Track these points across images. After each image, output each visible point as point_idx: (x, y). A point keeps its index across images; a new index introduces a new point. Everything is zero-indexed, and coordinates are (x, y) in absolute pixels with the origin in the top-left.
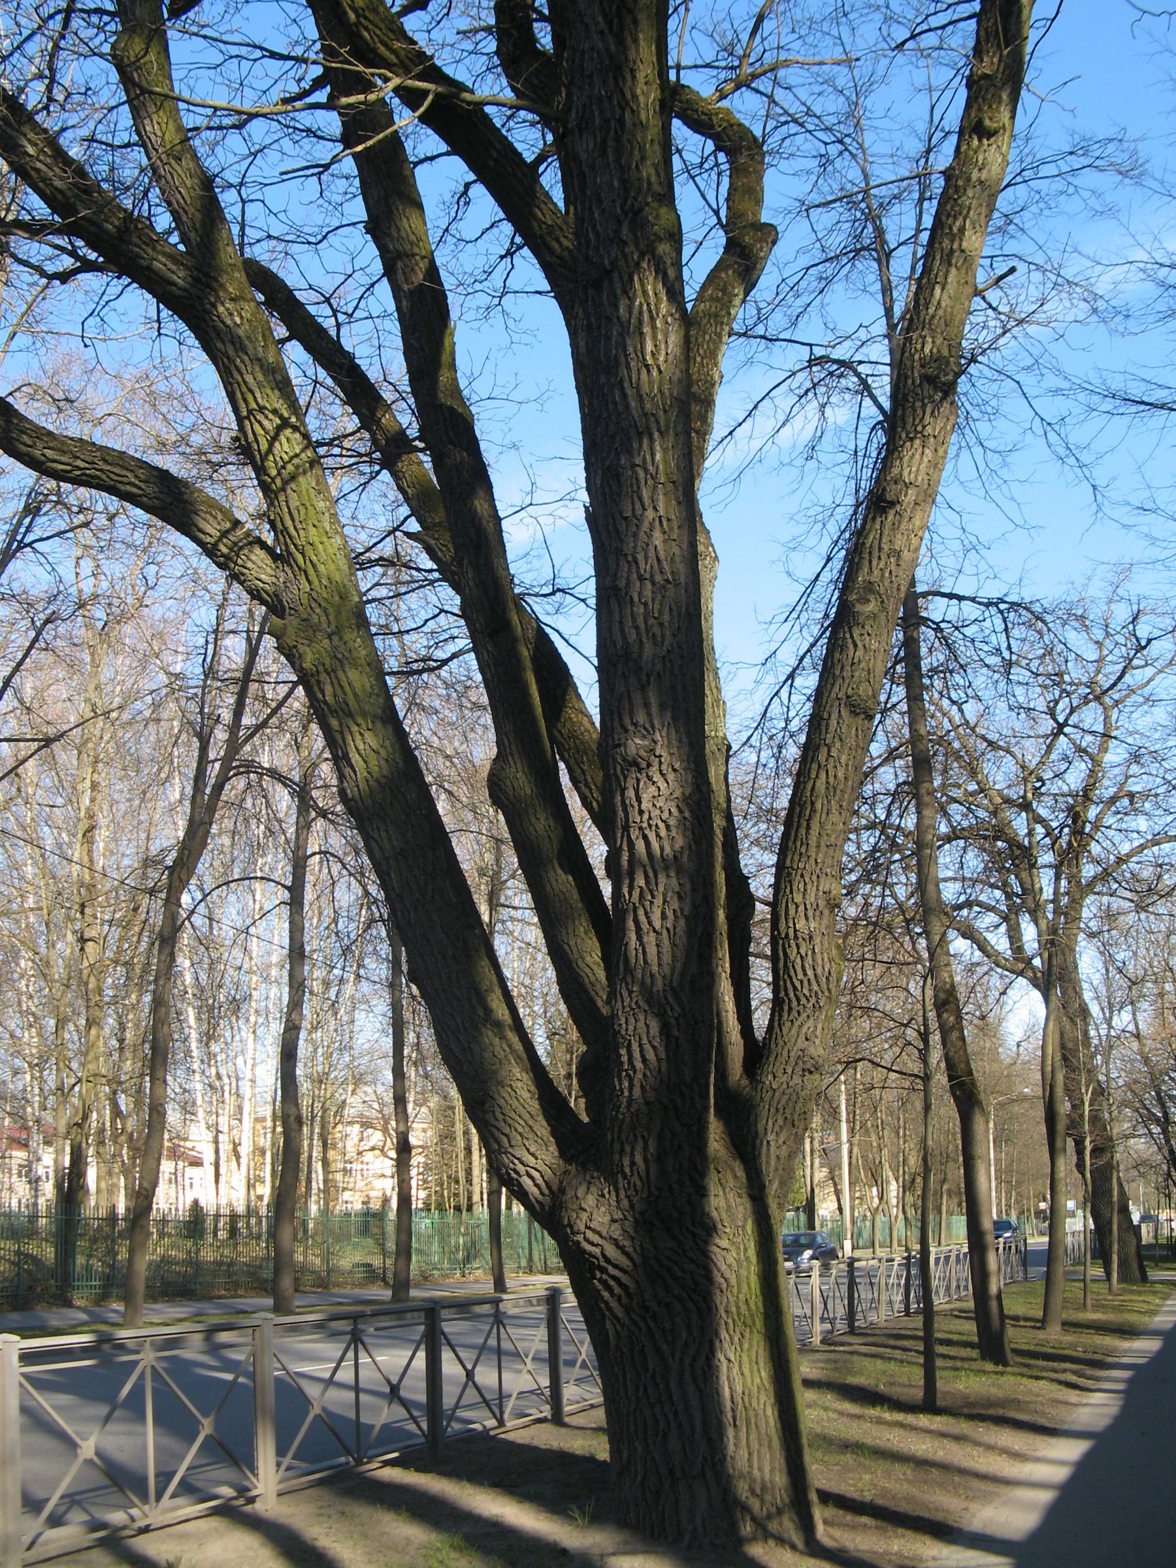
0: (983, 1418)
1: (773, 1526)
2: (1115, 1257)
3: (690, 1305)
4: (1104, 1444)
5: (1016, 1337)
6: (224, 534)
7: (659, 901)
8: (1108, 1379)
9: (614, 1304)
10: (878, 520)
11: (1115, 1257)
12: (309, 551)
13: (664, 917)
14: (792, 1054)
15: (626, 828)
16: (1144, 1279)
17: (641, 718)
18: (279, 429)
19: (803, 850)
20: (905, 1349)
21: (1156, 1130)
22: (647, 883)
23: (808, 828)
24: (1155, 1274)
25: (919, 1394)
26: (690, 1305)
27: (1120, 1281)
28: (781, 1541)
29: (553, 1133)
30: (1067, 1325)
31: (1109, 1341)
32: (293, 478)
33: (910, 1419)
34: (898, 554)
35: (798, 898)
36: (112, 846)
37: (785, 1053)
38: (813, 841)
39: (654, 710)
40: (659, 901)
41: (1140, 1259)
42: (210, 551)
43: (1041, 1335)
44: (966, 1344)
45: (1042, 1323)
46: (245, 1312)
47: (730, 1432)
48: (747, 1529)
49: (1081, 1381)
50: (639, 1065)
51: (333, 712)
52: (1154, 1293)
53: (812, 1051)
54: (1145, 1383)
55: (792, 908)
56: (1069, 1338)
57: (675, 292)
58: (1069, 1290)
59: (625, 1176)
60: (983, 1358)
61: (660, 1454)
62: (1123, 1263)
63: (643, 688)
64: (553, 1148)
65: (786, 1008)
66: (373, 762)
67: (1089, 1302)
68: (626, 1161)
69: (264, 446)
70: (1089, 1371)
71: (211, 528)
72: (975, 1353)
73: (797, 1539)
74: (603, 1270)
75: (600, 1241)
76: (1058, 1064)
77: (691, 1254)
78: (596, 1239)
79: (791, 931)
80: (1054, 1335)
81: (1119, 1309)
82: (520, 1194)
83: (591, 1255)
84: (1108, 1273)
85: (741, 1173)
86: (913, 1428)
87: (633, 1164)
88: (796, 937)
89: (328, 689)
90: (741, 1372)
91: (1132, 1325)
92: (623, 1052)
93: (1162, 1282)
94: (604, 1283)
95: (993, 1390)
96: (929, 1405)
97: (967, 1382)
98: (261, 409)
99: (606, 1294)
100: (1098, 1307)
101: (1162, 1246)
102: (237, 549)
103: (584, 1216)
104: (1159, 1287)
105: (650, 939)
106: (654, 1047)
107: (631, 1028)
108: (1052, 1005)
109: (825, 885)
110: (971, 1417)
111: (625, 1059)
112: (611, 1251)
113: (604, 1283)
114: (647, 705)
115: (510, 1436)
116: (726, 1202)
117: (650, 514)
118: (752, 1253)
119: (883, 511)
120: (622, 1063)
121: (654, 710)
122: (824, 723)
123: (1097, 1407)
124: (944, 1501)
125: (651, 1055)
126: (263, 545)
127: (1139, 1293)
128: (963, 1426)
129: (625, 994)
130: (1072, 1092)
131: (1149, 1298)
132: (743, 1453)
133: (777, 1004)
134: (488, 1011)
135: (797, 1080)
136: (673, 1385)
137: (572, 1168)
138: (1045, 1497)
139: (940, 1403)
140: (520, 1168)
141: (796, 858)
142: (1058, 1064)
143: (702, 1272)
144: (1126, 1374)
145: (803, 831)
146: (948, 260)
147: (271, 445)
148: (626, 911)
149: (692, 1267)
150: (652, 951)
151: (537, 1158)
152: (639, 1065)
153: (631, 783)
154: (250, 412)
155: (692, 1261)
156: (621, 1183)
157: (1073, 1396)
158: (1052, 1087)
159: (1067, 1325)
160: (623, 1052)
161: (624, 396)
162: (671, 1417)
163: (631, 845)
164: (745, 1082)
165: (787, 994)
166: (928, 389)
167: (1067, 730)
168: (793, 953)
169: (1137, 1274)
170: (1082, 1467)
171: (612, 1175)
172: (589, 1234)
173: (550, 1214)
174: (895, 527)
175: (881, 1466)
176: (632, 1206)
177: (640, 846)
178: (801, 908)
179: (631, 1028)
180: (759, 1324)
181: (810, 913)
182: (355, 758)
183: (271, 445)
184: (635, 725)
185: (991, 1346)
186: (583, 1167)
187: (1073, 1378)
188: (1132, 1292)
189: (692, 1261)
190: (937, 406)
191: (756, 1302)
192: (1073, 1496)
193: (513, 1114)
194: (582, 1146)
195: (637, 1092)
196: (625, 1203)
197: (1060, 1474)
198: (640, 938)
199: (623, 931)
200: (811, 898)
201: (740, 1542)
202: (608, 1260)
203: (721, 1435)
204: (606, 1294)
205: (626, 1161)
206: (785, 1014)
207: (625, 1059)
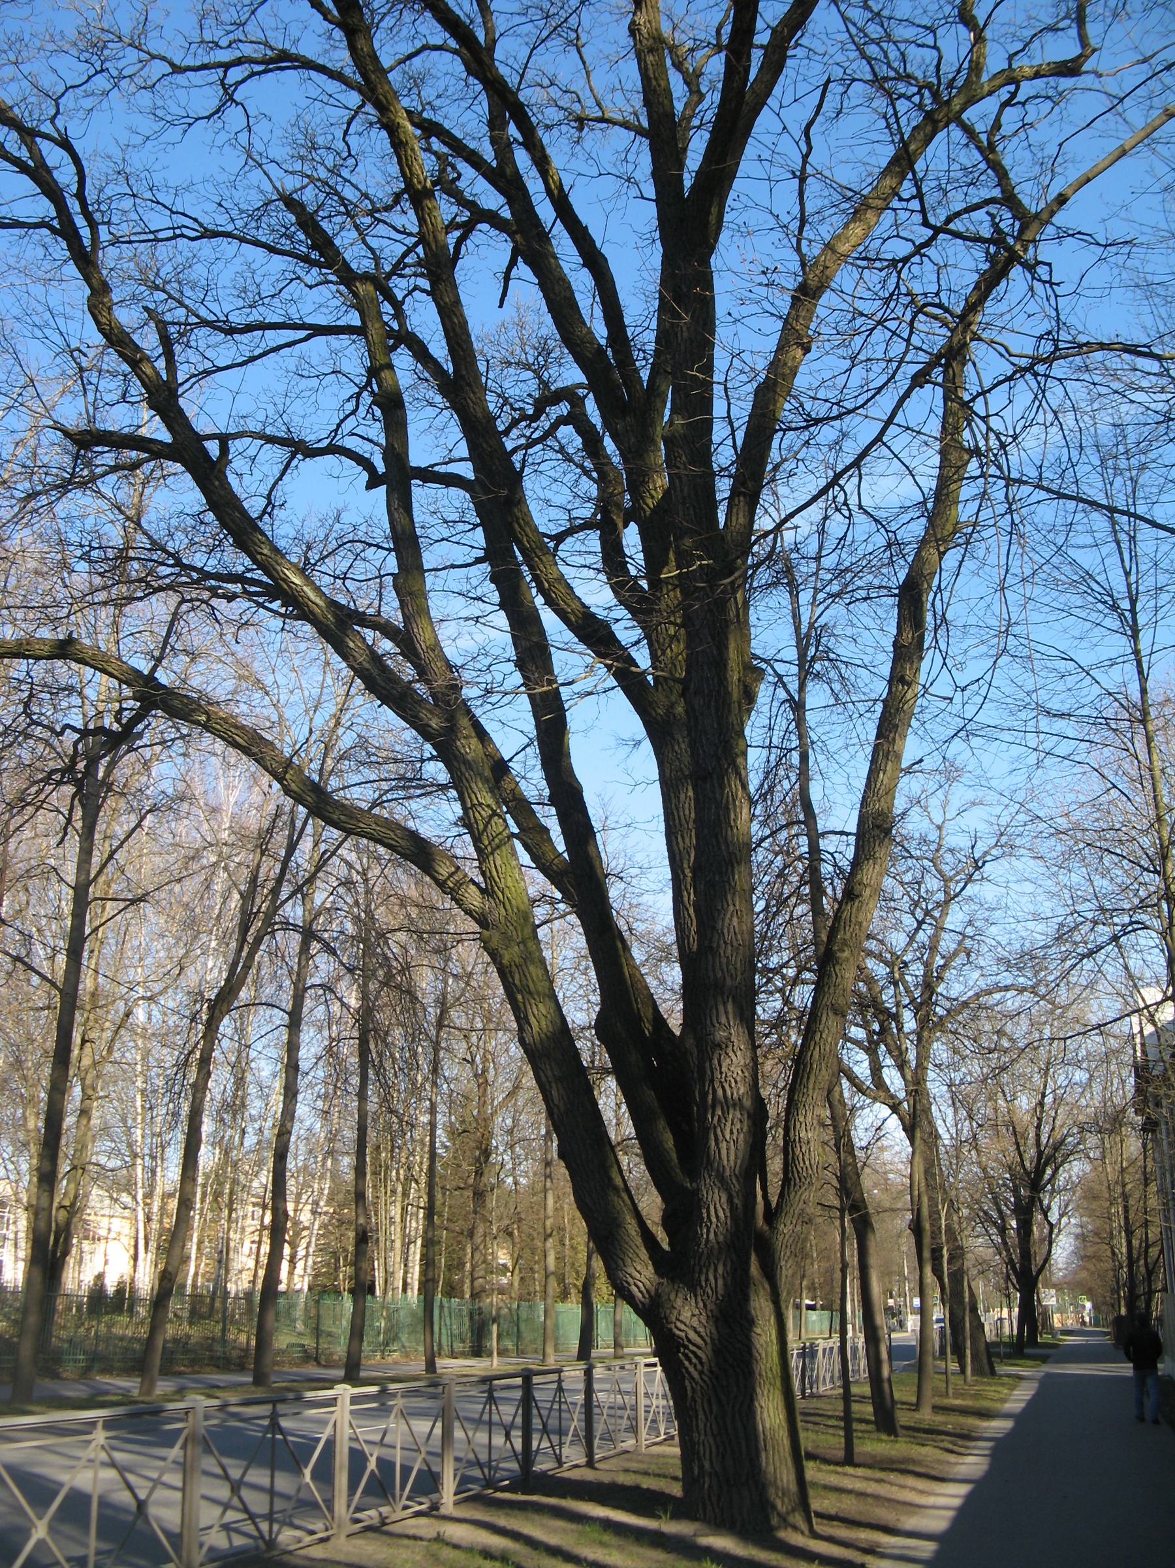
0: (893, 1470)
1: (791, 1519)
2: (968, 1352)
4: (981, 1489)
5: (903, 1417)
6: (451, 875)
7: (729, 1124)
8: (975, 1448)
9: (691, 1369)
11: (968, 1352)
12: (507, 891)
13: (731, 1132)
15: (712, 1081)
16: (993, 1373)
17: (723, 1020)
18: (491, 817)
20: (815, 1423)
21: (993, 1231)
24: (1003, 1369)
25: (841, 1454)
27: (973, 1374)
28: (795, 1528)
29: (651, 1258)
30: (937, 1409)
31: (972, 1421)
32: (498, 847)
33: (839, 1469)
34: (860, 924)
38: (811, 1086)
39: (731, 1016)
40: (729, 1124)
41: (989, 1355)
42: (441, 885)
43: (917, 1415)
44: (867, 1422)
45: (917, 1407)
46: (218, 1387)
47: (763, 1455)
48: (775, 1521)
49: (956, 1448)
50: (714, 1219)
51: (519, 991)
52: (1003, 1385)
53: (808, 1210)
54: (1002, 1449)
56: (939, 1418)
57: (745, 786)
58: (934, 1381)
60: (878, 1430)
61: (723, 1467)
62: (975, 1357)
63: (725, 1004)
64: (651, 1268)
66: (543, 1023)
67: (951, 1392)
68: (703, 1278)
69: (481, 827)
70: (960, 1442)
71: (444, 870)
72: (871, 1427)
73: (804, 1526)
74: (686, 1347)
76: (923, 1189)
78: (682, 1327)
80: (926, 1416)
81: (977, 1396)
82: (630, 1300)
84: (963, 1371)
85: (767, 1286)
86: (845, 1474)
87: (707, 1280)
89: (517, 977)
90: (770, 1412)
91: (988, 1409)
93: (1009, 1376)
94: (686, 1355)
95: (893, 1453)
96: (849, 1459)
97: (872, 1445)
98: (480, 804)
99: (686, 1363)
100: (957, 1395)
101: (1005, 1344)
102: (459, 884)
104: (1006, 1380)
105: (724, 1145)
108: (918, 1142)
109: (818, 1111)
110: (883, 1469)
112: (692, 1335)
113: (686, 1355)
114: (726, 1013)
115: (566, 1475)
116: (761, 1305)
117: (731, 908)
118: (774, 1337)
119: (853, 900)
121: (731, 1016)
123: (973, 1463)
124: (886, 1515)
125: (721, 1214)
126: (474, 883)
127: (989, 1384)
128: (879, 1475)
130: (935, 1215)
131: (1000, 1389)
132: (771, 1469)
133: (787, 1181)
134: (610, 1179)
135: (798, 1228)
137: (665, 1281)
138: (951, 1514)
139: (856, 1460)
142: (923, 1189)
144: (990, 1444)
146: (886, 756)
147: (486, 827)
150: (724, 1152)
151: (642, 1274)
152: (714, 1219)
153: (716, 1056)
154: (473, 805)
156: (699, 1291)
157: (952, 1458)
158: (919, 1210)
159: (937, 1409)
161: (718, 842)
164: (766, 1228)
166: (876, 832)
167: (924, 926)
169: (987, 1367)
170: (969, 1499)
171: (693, 1287)
173: (653, 1314)
174: (859, 909)
175: (833, 1496)
176: (705, 1306)
177: (720, 1092)
180: (778, 1383)
182: (532, 1020)
183: (486, 827)
185: (885, 1422)
186: (672, 1280)
187: (950, 1446)
188: (983, 1383)
190: (882, 842)
191: (777, 1369)
192: (965, 1514)
194: (677, 1265)
195: (712, 1236)
196: (701, 1304)
197: (957, 1502)
198: (717, 1144)
199: (708, 1139)
200: (809, 1119)
201: (772, 1529)
202: (689, 1341)
203: (758, 1456)
204: (686, 1363)
205: (703, 1278)
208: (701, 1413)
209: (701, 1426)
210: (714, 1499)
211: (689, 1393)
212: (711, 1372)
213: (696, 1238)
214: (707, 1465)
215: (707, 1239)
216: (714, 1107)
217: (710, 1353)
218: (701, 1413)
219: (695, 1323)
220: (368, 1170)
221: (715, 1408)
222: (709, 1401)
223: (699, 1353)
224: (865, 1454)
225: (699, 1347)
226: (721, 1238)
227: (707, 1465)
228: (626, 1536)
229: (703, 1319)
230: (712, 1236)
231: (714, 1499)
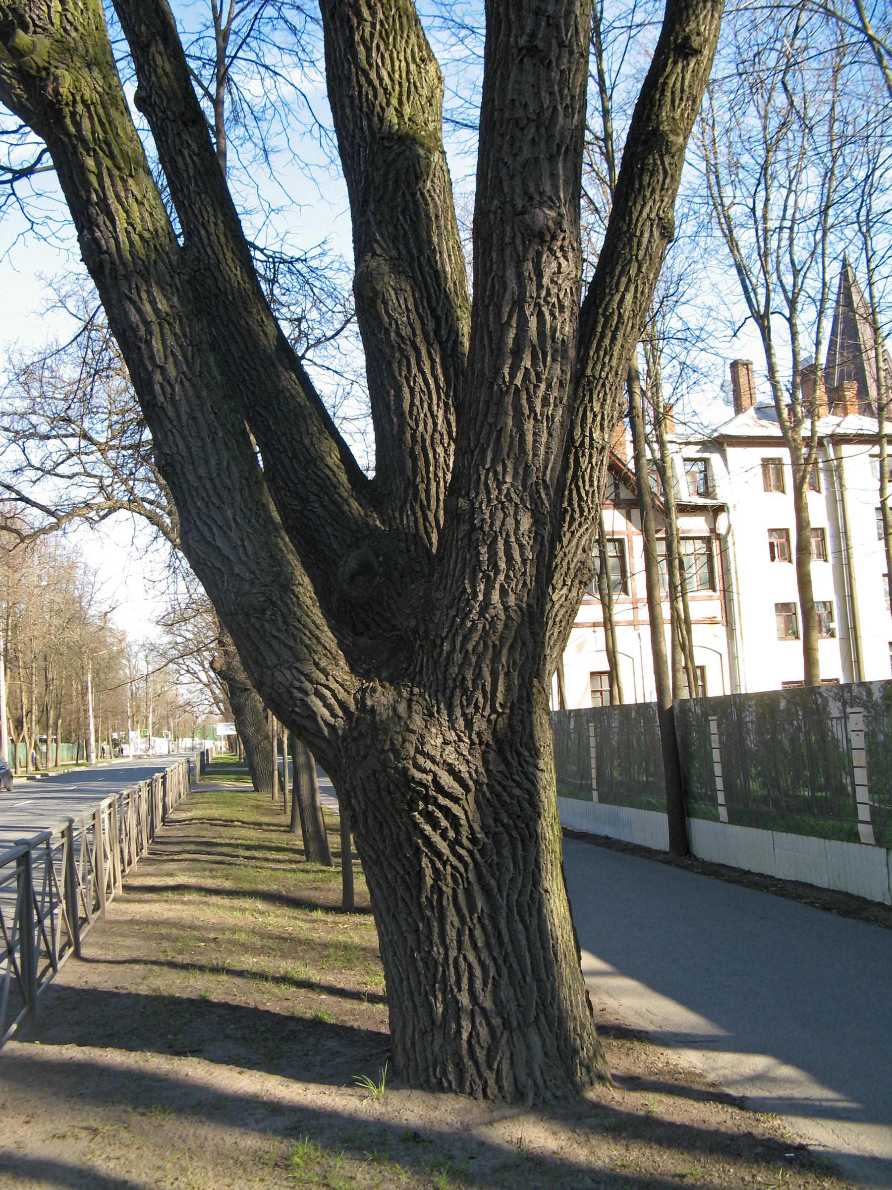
3: (515, 834)
9: (436, 838)
10: (680, 65)
13: (545, 402)
14: (572, 566)
15: (519, 303)
19: (607, 360)
22: (534, 364)
23: (614, 339)
26: (515, 834)
35: (597, 409)
36: (518, 134)
37: (565, 564)
55: (590, 416)
59: (465, 691)
63: (552, 158)
65: (568, 518)
74: (427, 799)
75: (434, 768)
77: (517, 778)
78: (429, 765)
79: (587, 440)
83: (421, 783)
87: (478, 675)
88: (591, 446)
92: (483, 550)
103: (413, 738)
105: (529, 426)
106: (521, 546)
107: (498, 523)
111: (485, 557)
112: (446, 780)
114: (554, 175)
120: (479, 563)
122: (635, 240)
129: (492, 484)
136: (503, 924)
140: (308, 686)
141: (599, 367)
143: (527, 796)
145: (607, 341)
148: (503, 394)
149: (517, 791)
152: (503, 565)
155: (518, 785)
160: (483, 550)
162: (500, 961)
163: (523, 322)
165: (570, 504)
168: (584, 462)
172: (421, 760)
176: (469, 725)
178: (599, 418)
179: (498, 523)
181: (606, 423)
184: (541, 194)
189: (518, 785)
193: (297, 624)
196: (461, 722)
201: (578, 1090)
202: (439, 788)
206: (566, 525)
207: (485, 557)
208: (452, 916)
209: (451, 933)
210: (481, 1055)
211: (429, 881)
212: (473, 840)
213: (460, 602)
214: (464, 999)
215: (486, 604)
216: (517, 354)
217: (471, 808)
218: (452, 916)
219: (450, 756)
220: (91, 713)
221: (480, 904)
222: (468, 892)
223: (456, 809)
224: (845, 677)
225: (456, 800)
226: (512, 600)
227: (464, 999)
228: (708, 1100)
229: (464, 748)
230: (495, 596)
231: (481, 1055)
